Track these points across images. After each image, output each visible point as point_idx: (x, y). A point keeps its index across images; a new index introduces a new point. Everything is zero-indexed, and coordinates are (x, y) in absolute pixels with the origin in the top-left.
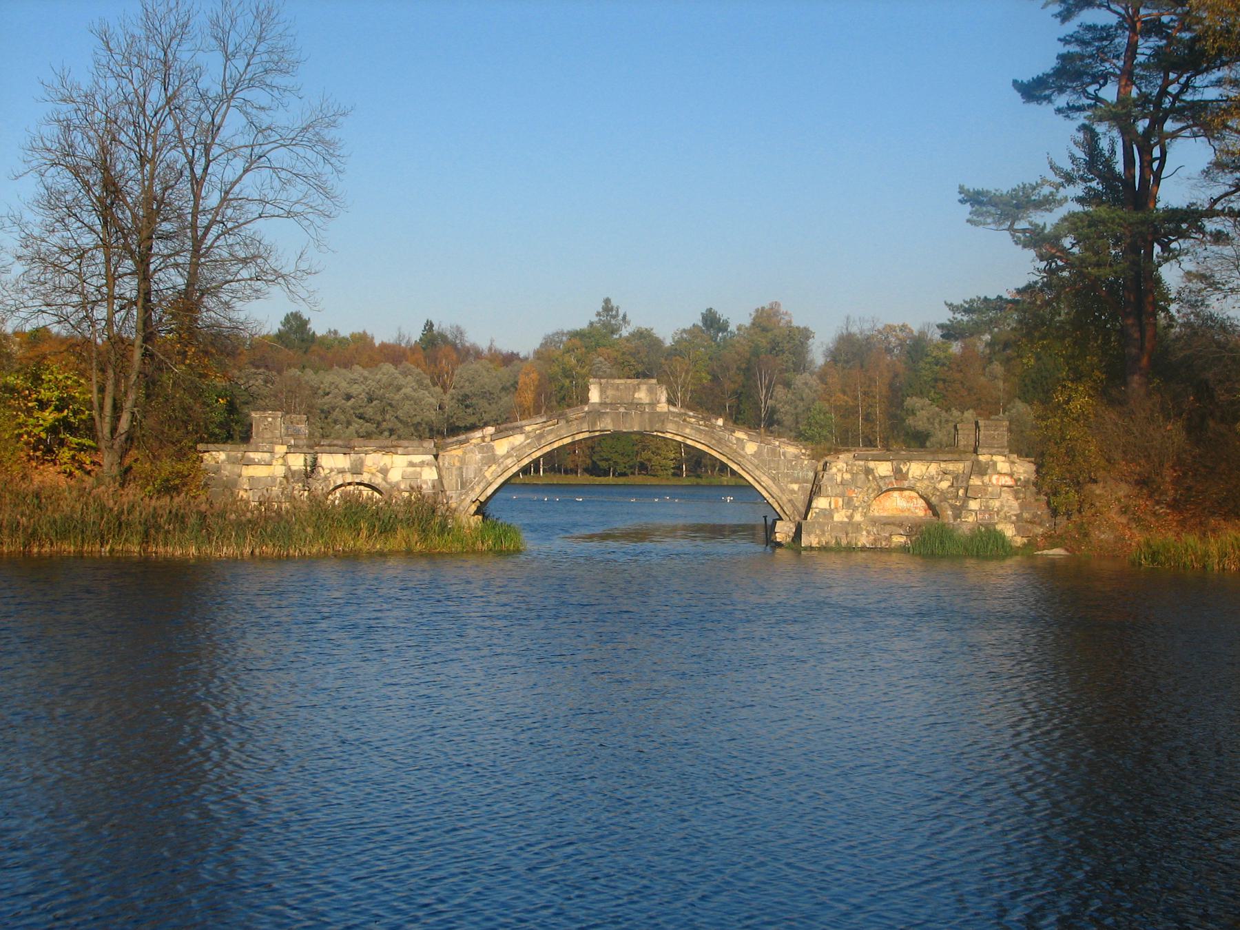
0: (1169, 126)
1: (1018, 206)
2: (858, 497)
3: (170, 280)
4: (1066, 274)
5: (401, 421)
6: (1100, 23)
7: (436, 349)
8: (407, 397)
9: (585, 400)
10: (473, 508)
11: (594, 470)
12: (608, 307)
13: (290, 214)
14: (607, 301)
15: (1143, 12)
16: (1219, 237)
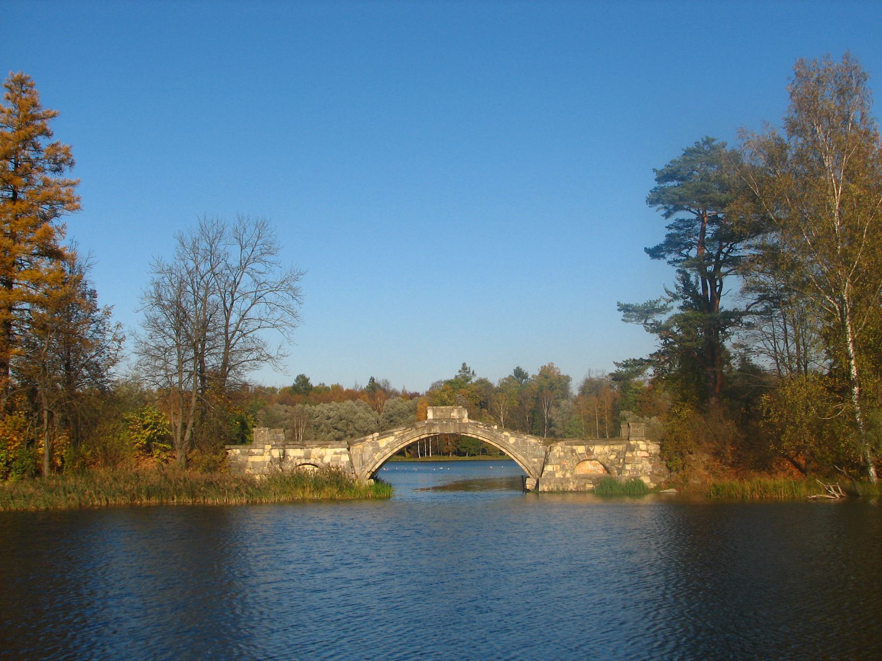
0: (723, 270)
1: (647, 312)
2: (568, 464)
3: (212, 361)
4: (676, 346)
5: (357, 430)
6: (686, 218)
7: (375, 392)
8: (360, 418)
9: (426, 417)
10: (369, 475)
11: (459, 453)
12: (464, 367)
13: (274, 326)
14: (464, 364)
15: (708, 212)
16: (749, 326)
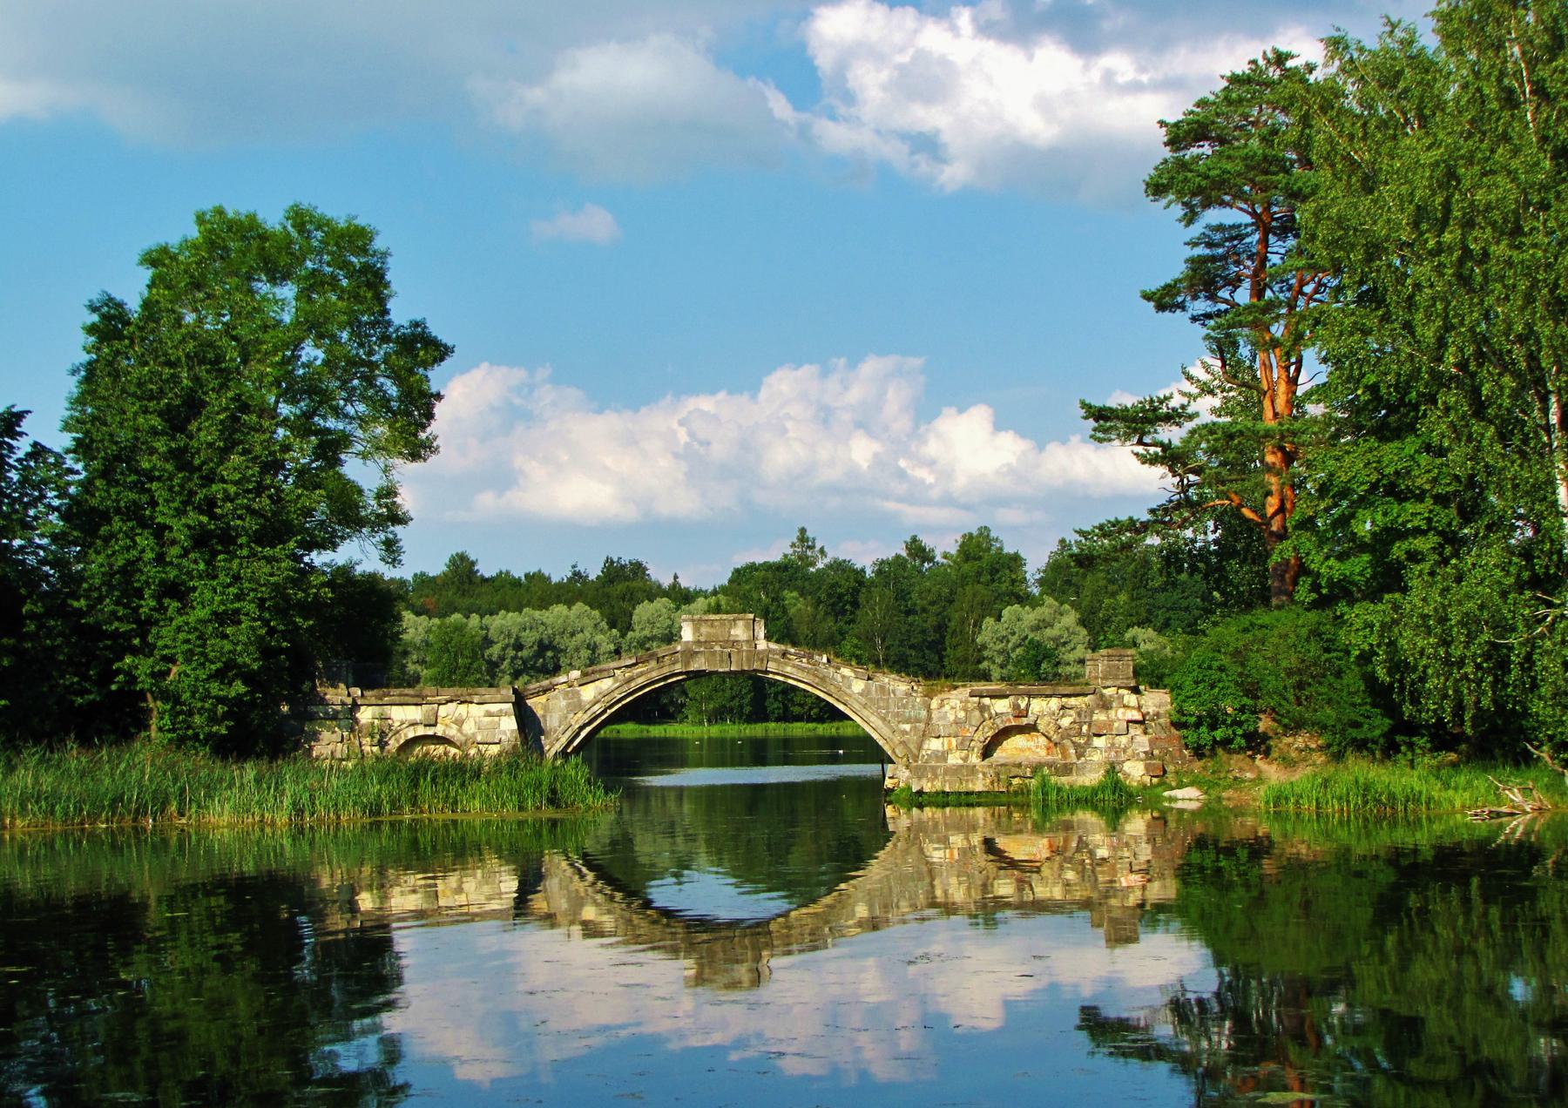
6: (1228, 222)
14: (803, 531)
